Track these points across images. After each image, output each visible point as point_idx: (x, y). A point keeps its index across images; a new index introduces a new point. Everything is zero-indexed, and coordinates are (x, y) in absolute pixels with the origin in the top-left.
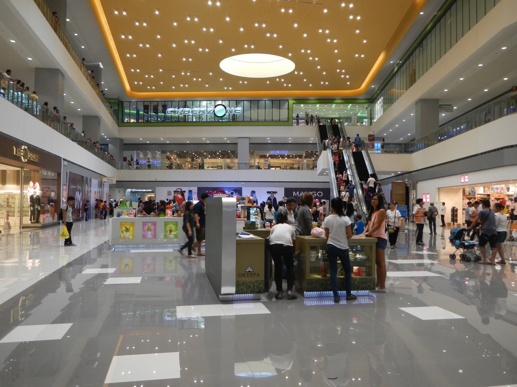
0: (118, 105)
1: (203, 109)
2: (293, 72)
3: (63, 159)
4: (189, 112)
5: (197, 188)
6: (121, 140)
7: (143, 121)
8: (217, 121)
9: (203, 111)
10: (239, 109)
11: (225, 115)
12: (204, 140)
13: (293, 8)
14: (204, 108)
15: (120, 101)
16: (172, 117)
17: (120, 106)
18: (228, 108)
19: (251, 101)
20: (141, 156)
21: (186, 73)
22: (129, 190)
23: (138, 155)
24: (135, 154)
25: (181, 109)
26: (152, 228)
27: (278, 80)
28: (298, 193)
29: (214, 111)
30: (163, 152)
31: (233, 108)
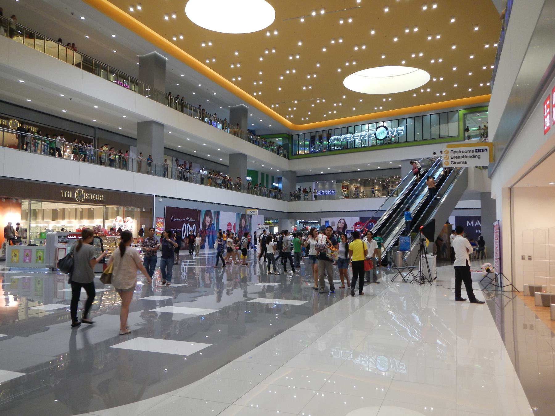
0: (289, 139)
1: (364, 133)
2: (431, 79)
3: (156, 196)
4: (350, 138)
5: (359, 218)
6: (293, 173)
7: (314, 153)
8: (387, 143)
9: (364, 136)
10: (402, 128)
11: (386, 137)
12: (369, 166)
13: (352, 17)
14: (367, 132)
15: (289, 135)
16: (335, 145)
17: (290, 140)
18: (389, 129)
19: (414, 118)
20: (320, 186)
21: (321, 100)
22: (298, 221)
23: (317, 185)
24: (313, 185)
25: (343, 136)
26: (29, 254)
27: (422, 91)
28: (472, 222)
29: (375, 134)
30: (338, 181)
31: (395, 129)
